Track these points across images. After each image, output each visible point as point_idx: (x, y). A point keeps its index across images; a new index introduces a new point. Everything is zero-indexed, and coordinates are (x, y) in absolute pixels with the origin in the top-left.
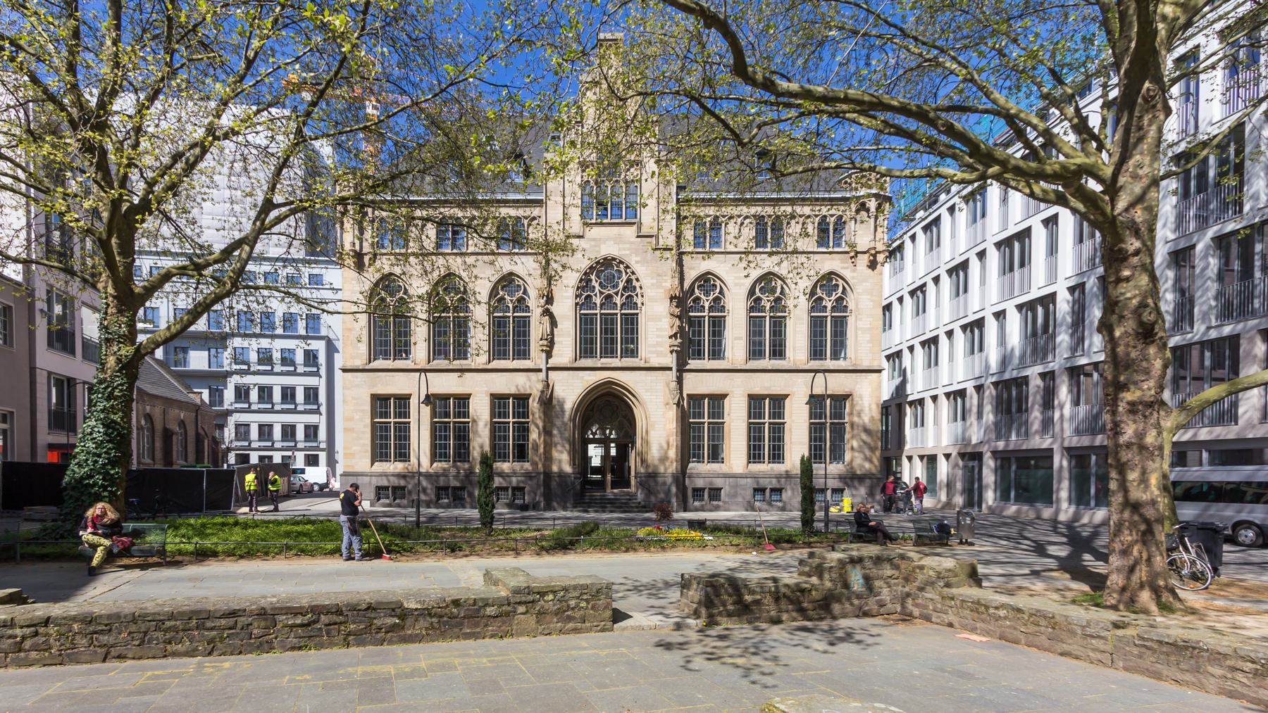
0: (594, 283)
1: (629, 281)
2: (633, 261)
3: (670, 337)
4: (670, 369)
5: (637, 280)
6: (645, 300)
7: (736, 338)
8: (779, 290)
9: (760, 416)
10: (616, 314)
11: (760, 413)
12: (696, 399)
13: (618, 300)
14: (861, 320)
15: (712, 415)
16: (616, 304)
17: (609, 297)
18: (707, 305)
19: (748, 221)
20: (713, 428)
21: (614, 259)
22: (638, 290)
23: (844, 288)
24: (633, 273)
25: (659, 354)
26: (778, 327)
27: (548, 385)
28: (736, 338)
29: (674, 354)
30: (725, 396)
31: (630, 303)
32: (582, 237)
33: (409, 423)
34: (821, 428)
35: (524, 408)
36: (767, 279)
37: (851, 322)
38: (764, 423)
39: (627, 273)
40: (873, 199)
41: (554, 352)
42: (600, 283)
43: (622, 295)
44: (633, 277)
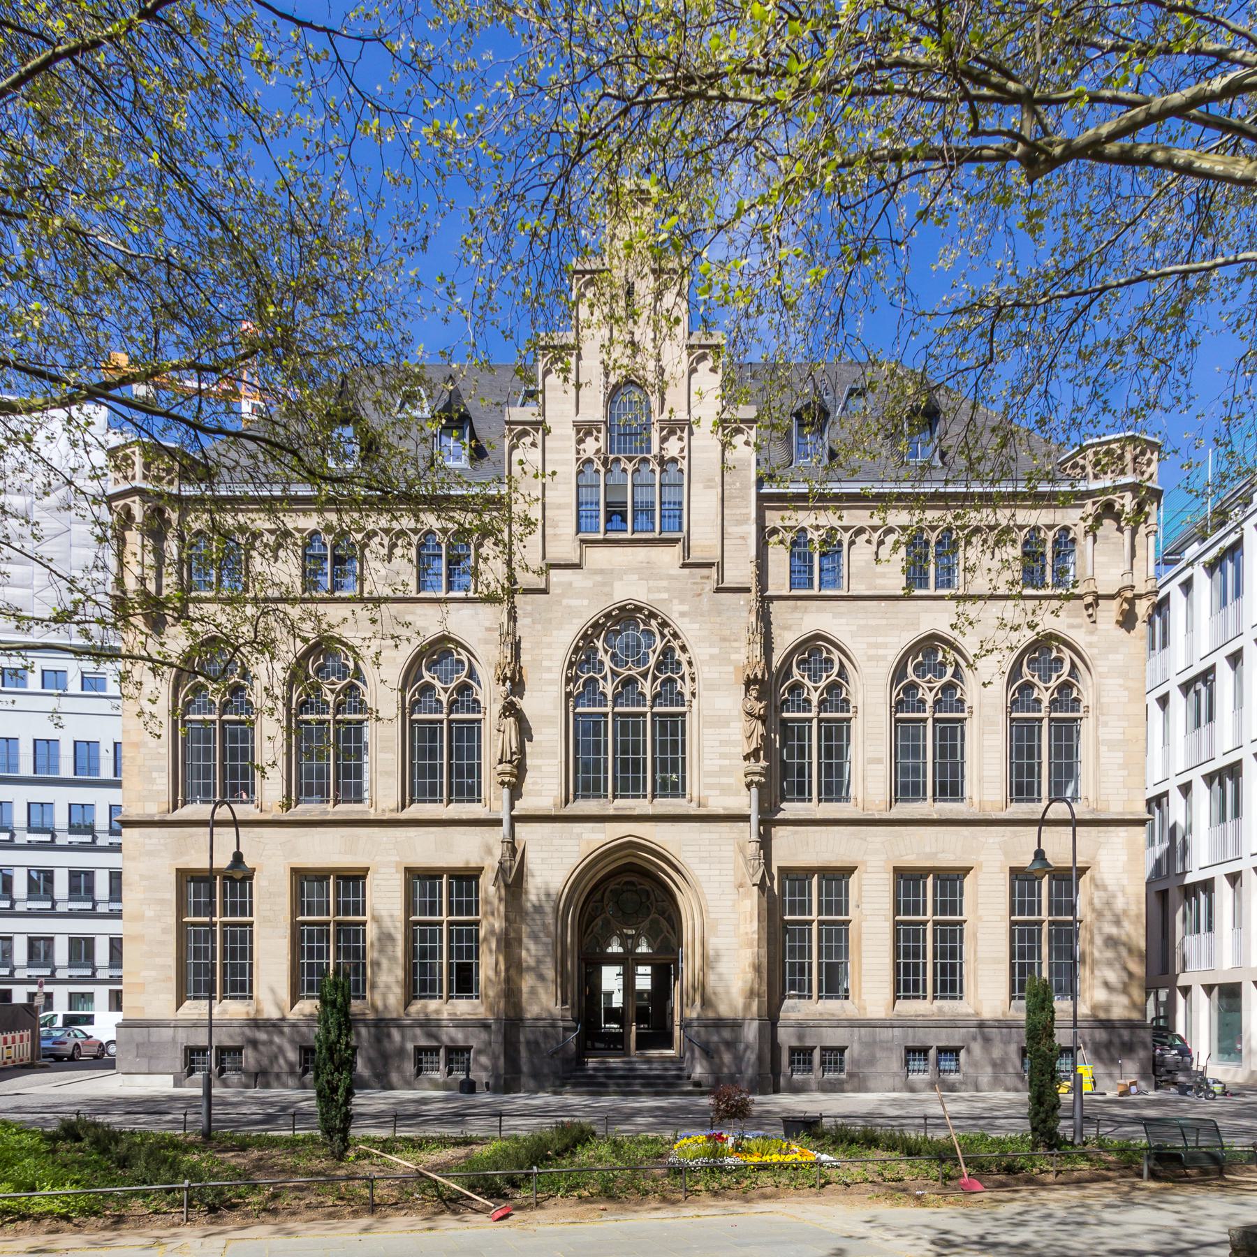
1: (667, 651)
2: (675, 612)
3: (747, 758)
5: (683, 648)
10: (644, 714)
12: (796, 877)
13: (647, 688)
16: (642, 694)
17: (629, 682)
21: (639, 609)
22: (685, 667)
24: (675, 635)
25: (725, 790)
30: (847, 872)
31: (669, 692)
32: (577, 566)
33: (251, 924)
37: (1087, 730)
38: (924, 923)
39: (663, 636)
41: (527, 786)
43: (655, 678)
44: (675, 644)
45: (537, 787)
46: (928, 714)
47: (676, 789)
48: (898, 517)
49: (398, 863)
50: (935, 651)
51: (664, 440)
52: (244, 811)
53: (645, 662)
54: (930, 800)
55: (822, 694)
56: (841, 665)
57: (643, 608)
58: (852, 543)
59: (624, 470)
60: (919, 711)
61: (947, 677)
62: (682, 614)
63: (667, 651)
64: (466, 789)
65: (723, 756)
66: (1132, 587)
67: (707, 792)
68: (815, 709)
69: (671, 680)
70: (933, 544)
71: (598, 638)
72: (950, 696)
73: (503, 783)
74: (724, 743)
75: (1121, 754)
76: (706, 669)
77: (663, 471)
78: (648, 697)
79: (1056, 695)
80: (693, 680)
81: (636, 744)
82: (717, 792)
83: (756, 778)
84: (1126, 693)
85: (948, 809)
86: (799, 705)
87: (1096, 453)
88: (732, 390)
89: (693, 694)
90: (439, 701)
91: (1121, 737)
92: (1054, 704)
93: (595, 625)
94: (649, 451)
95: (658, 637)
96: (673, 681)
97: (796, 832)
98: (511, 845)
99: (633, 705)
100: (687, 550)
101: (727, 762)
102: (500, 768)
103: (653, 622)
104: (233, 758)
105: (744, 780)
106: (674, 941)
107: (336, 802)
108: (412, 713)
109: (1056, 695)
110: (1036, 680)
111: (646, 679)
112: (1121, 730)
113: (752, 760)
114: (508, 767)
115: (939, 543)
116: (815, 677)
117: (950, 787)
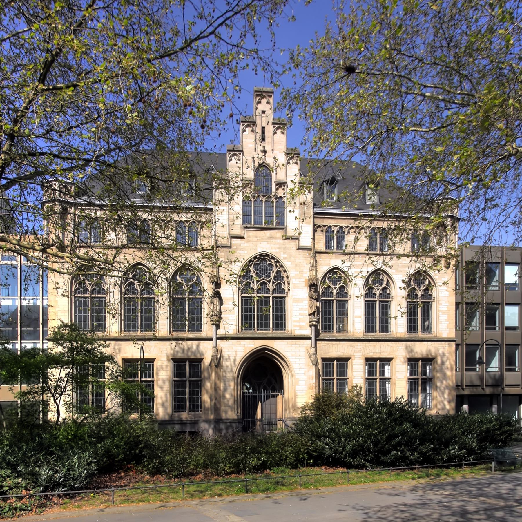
0: (252, 273)
1: (278, 272)
2: (281, 256)
3: (310, 315)
4: (310, 338)
5: (285, 271)
6: (291, 286)
7: (356, 317)
8: (385, 282)
9: (331, 373)
10: (269, 297)
11: (330, 372)
12: (327, 361)
13: (271, 286)
14: (441, 304)
15: (339, 373)
16: (268, 289)
17: (264, 283)
18: (335, 292)
19: (353, 230)
20: (340, 383)
21: (267, 255)
22: (285, 279)
23: (429, 282)
24: (282, 266)
25: (301, 327)
26: (385, 307)
27: (217, 351)
28: (356, 317)
29: (313, 328)
30: (347, 359)
31: (279, 289)
32: (242, 238)
33: (153, 381)
34: (330, 383)
35: (197, 369)
36: (377, 273)
37: (434, 305)
38: (333, 379)
39: (277, 266)
40: (449, 219)
41: (221, 326)
42: (257, 273)
43: (273, 283)
44: (281, 269)
48: (365, 223)
50: (380, 274)
51: (277, 189)
53: (269, 276)
54: (378, 332)
56: (388, 281)
58: (349, 232)
59: (262, 201)
61: (384, 285)
62: (285, 258)
64: (196, 325)
65: (300, 314)
67: (295, 328)
69: (279, 284)
70: (335, 232)
71: (251, 266)
72: (385, 293)
73: (213, 324)
74: (301, 309)
76: (293, 280)
77: (277, 202)
78: (271, 290)
81: (330, 312)
82: (298, 328)
83: (314, 323)
85: (426, 336)
88: (303, 172)
90: (136, 290)
93: (250, 261)
94: (271, 193)
95: (275, 267)
96: (250, 283)
97: (328, 344)
98: (217, 350)
100: (286, 232)
103: (272, 261)
104: (146, 313)
105: (309, 324)
107: (141, 331)
108: (76, 293)
110: (416, 287)
114: (215, 318)
115: (338, 231)
116: (335, 284)
117: (385, 327)
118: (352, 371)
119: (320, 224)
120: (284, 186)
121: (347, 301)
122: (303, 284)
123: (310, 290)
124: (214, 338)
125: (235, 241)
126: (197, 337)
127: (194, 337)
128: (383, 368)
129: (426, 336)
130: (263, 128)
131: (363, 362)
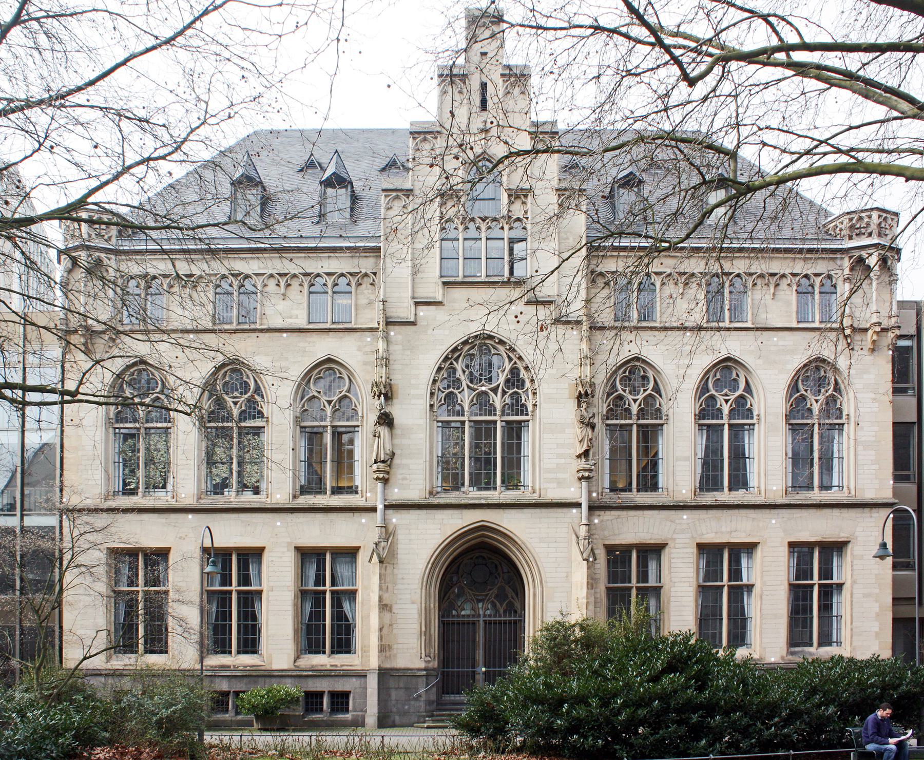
1: (514, 371)
3: (579, 456)
4: (578, 505)
13: (497, 401)
22: (528, 384)
24: (520, 358)
25: (560, 483)
31: (518, 406)
32: (439, 303)
39: (510, 359)
43: (504, 393)
44: (520, 365)
45: (405, 482)
46: (725, 421)
47: (512, 480)
49: (289, 544)
52: (161, 498)
55: (640, 405)
57: (494, 337)
59: (478, 228)
60: (717, 419)
63: (514, 371)
66: (880, 324)
67: (547, 485)
68: (634, 417)
73: (377, 479)
75: (873, 453)
79: (734, 406)
80: (535, 394)
84: (876, 405)
85: (739, 496)
86: (713, 414)
87: (851, 220)
89: (535, 405)
91: (873, 439)
92: (642, 413)
95: (507, 360)
99: (486, 415)
101: (563, 461)
102: (375, 467)
106: (518, 605)
109: (734, 406)
111: (496, 394)
112: (873, 434)
113: (583, 460)
116: (634, 391)
118: (670, 573)
119: (321, 271)
120: (526, 196)
121: (662, 425)
122: (566, 393)
123: (579, 406)
124: (380, 507)
125: (423, 311)
126: (347, 505)
127: (342, 505)
128: (738, 562)
129: (739, 496)
130: (484, 86)
131: (785, 550)
